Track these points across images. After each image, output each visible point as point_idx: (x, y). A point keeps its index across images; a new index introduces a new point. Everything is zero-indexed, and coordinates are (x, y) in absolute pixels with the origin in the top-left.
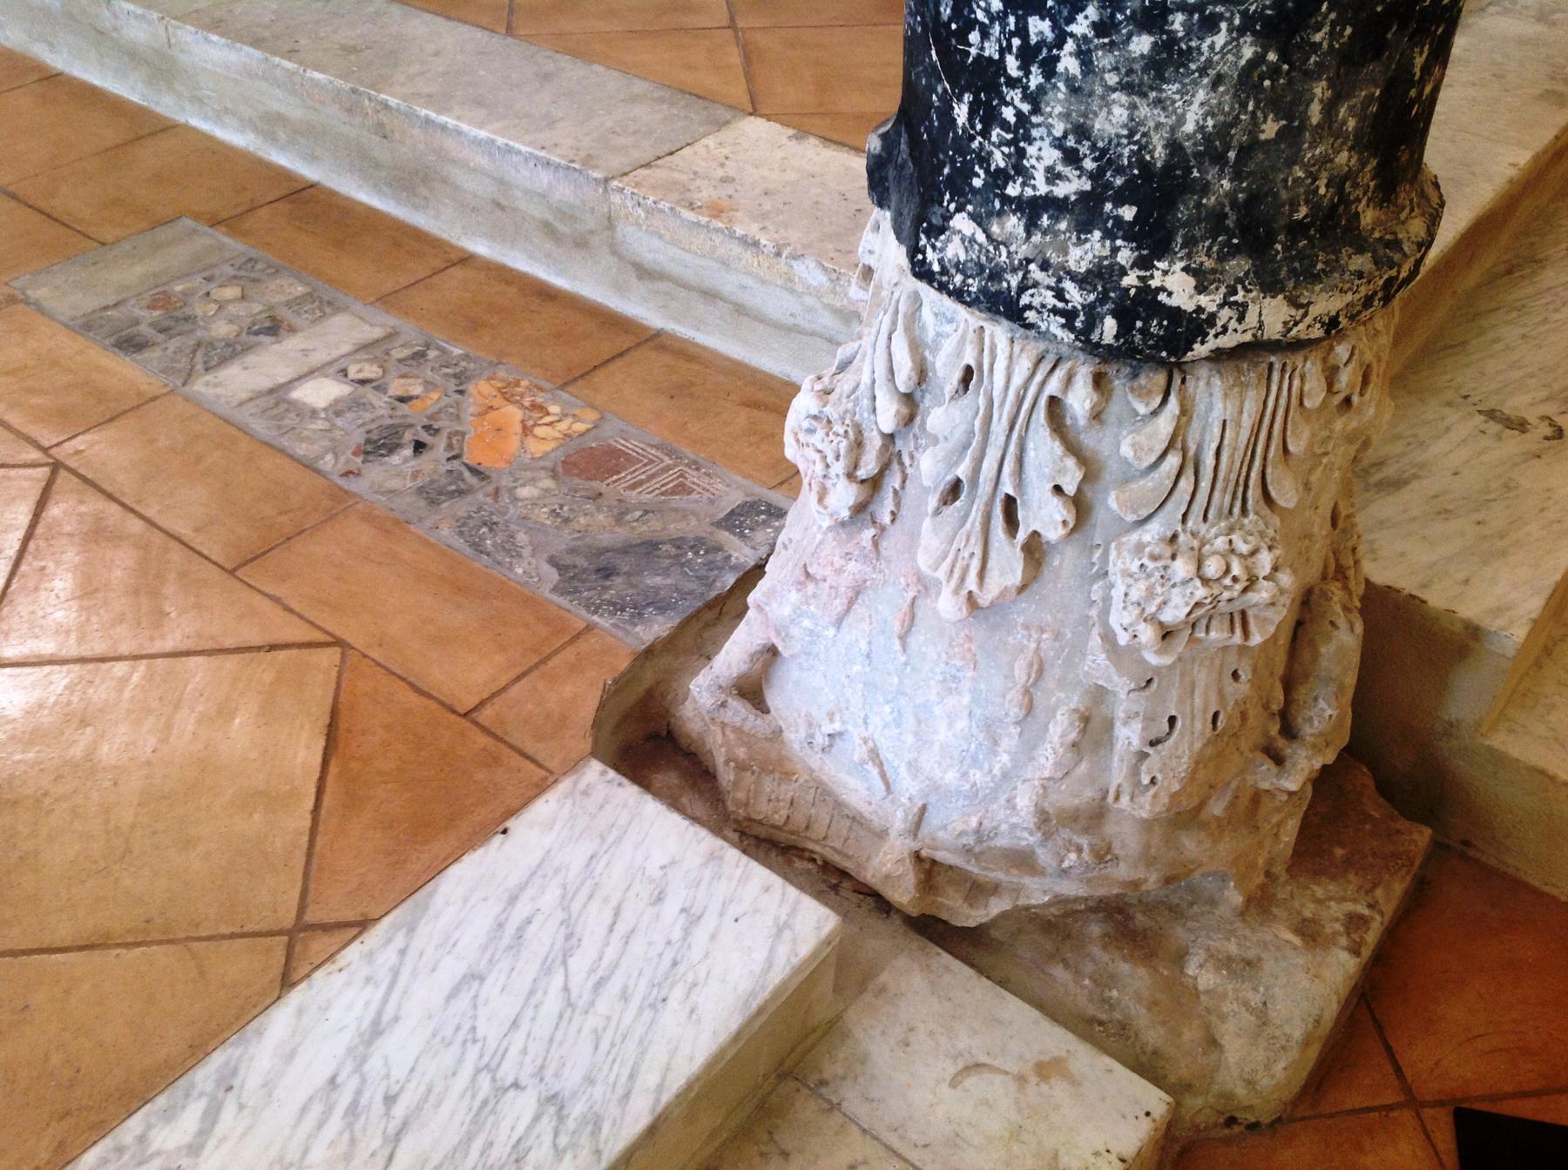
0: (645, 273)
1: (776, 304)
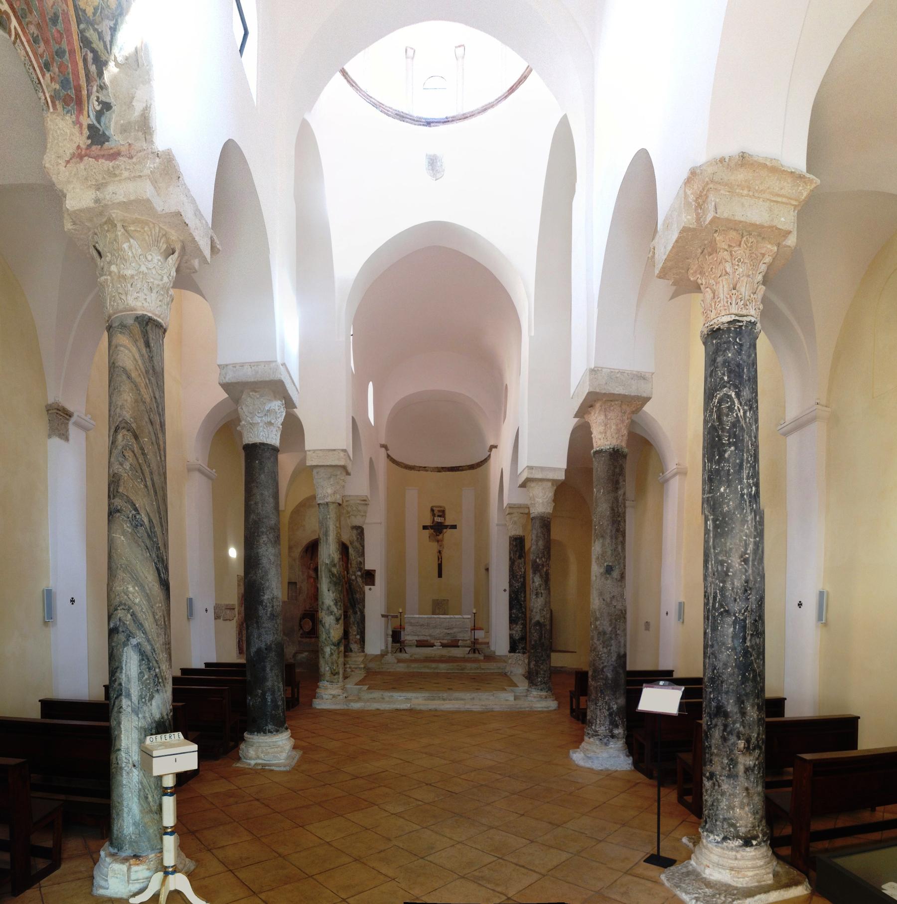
0: (483, 669)
1: (492, 668)
